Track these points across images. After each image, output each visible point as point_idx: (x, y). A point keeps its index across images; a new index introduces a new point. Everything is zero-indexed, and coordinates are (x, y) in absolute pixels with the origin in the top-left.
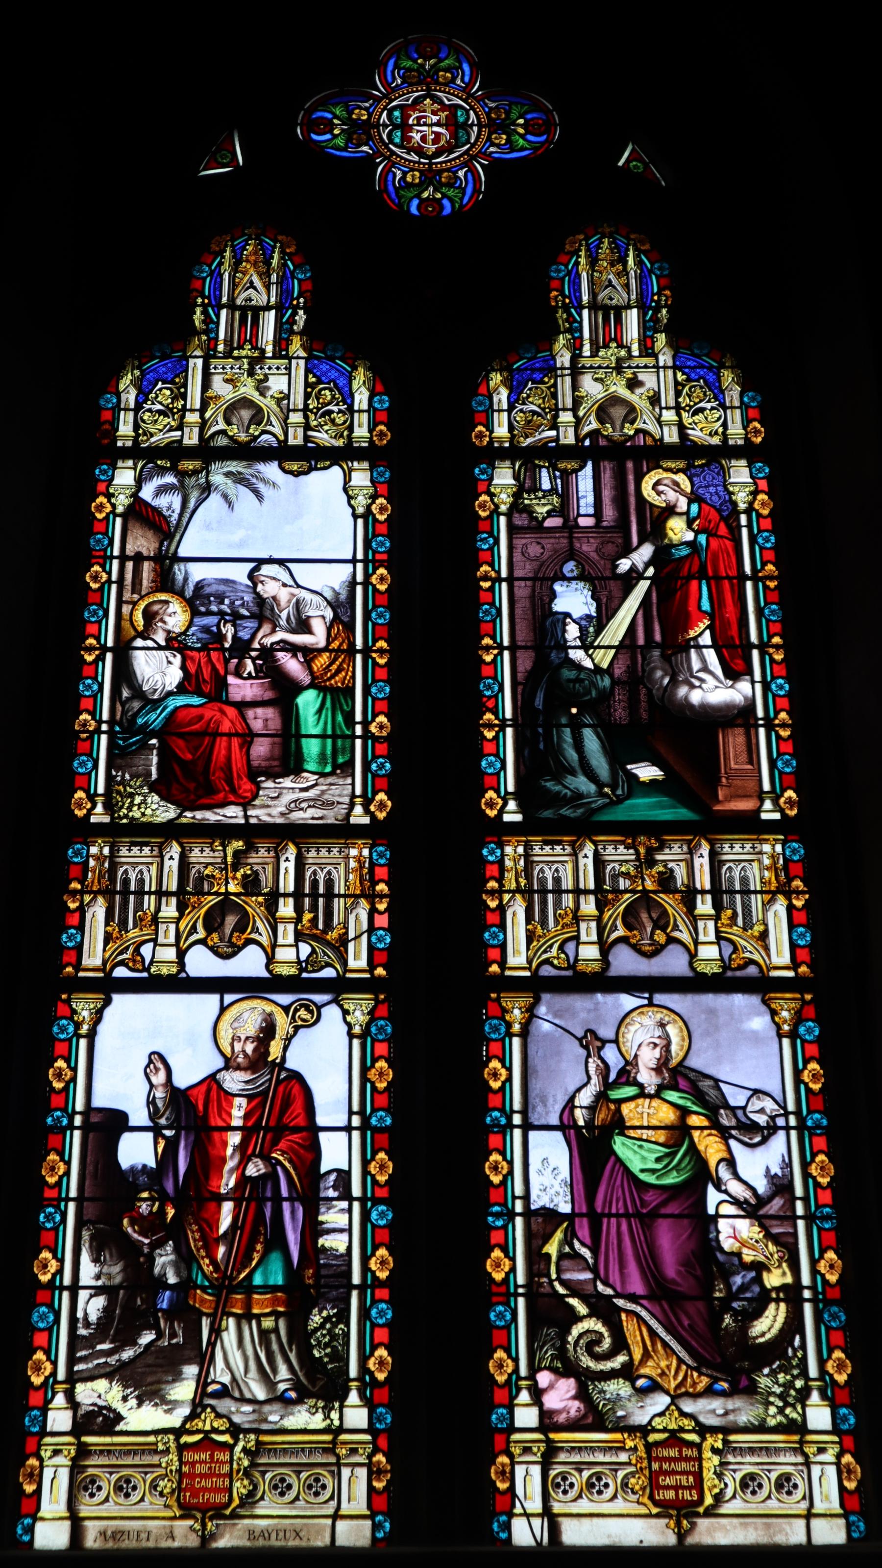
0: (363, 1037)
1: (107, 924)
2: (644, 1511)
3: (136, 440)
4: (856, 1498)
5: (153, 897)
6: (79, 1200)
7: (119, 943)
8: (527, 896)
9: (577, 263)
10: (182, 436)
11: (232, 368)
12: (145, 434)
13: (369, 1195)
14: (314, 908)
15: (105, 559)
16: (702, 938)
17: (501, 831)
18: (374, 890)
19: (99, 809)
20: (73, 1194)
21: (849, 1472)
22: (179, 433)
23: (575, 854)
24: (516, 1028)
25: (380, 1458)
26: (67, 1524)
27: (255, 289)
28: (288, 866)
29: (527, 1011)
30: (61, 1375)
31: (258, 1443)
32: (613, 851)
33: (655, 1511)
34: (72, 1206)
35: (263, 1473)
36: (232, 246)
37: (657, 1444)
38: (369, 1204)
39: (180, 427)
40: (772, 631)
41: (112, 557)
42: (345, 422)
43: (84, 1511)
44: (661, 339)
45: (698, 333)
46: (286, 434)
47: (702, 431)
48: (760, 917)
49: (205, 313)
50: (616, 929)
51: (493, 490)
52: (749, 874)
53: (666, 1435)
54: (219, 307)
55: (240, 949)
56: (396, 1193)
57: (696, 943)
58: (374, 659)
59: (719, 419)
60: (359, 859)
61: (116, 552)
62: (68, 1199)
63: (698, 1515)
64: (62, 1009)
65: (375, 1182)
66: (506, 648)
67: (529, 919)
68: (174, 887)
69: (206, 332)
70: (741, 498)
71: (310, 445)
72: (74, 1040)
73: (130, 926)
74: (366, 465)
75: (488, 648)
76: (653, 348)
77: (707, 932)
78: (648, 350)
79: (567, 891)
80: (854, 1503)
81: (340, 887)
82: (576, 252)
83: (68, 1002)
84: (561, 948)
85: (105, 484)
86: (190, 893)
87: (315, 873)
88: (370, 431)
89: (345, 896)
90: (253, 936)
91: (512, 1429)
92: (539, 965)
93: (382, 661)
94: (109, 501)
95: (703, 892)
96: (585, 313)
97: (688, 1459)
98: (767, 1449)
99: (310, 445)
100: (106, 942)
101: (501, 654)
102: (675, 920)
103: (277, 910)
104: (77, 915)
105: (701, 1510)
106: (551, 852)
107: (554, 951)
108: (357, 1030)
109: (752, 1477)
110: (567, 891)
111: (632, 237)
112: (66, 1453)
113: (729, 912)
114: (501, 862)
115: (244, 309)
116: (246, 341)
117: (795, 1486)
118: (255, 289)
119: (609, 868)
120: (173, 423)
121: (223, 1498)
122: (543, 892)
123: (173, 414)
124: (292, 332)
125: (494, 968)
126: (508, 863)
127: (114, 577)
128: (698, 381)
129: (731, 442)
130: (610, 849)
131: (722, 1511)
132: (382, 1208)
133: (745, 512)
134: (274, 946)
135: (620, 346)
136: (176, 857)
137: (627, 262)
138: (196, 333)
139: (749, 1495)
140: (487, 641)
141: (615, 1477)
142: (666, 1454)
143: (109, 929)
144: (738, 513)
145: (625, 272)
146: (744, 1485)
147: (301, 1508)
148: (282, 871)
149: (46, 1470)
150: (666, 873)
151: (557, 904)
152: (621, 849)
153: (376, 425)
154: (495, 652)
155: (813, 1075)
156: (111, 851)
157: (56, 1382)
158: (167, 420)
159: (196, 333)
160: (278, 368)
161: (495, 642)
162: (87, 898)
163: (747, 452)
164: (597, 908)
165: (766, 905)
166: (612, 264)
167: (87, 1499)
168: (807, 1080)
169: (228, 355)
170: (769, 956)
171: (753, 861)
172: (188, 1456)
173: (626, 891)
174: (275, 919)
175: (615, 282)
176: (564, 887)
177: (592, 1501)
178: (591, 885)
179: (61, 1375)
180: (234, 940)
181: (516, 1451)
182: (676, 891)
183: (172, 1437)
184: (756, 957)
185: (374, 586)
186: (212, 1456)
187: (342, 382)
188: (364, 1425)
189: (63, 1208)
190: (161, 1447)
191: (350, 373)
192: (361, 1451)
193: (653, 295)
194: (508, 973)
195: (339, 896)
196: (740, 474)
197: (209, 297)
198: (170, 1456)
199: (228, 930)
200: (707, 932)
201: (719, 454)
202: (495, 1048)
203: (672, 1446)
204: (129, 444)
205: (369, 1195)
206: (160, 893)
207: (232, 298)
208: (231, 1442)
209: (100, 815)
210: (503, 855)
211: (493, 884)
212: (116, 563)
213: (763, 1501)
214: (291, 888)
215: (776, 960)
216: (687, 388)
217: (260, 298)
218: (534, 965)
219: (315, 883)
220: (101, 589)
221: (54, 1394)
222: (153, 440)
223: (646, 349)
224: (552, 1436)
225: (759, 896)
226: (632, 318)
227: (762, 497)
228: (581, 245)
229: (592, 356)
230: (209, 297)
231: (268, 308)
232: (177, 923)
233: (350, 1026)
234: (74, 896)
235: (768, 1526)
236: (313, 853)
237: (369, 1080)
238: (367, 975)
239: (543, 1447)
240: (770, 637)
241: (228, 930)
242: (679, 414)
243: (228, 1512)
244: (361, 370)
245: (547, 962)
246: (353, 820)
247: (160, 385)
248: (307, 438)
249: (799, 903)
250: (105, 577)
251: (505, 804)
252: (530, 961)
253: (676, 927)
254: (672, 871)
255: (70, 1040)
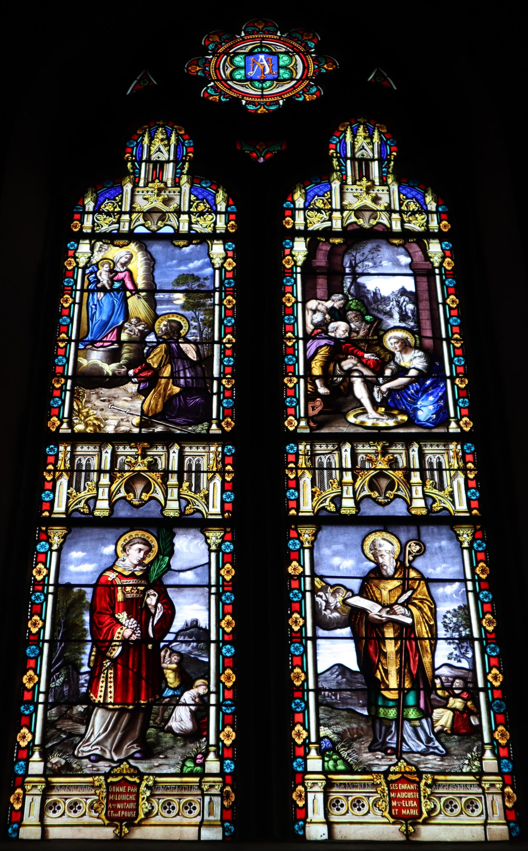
0: (217, 551)
1: (312, 487)
2: (385, 820)
3: (93, 228)
4: (513, 812)
5: (95, 473)
6: (52, 642)
7: (75, 499)
8: (69, 473)
9: (345, 137)
10: (119, 227)
11: (357, 190)
12: (98, 226)
13: (221, 639)
14: (189, 480)
15: (72, 291)
16: (414, 495)
17: (296, 437)
18: (224, 469)
19: (65, 426)
20: (47, 637)
21: (509, 797)
22: (117, 225)
23: (407, 450)
24: (55, 547)
25: (508, 790)
26: (39, 829)
27: (161, 152)
28: (174, 457)
29: (312, 536)
30: (313, 739)
31: (155, 782)
32: (123, 450)
33: (392, 820)
34: (46, 646)
35: (439, 798)
36: (351, 128)
37: (112, 783)
38: (221, 644)
39: (118, 222)
40: (227, 331)
41: (76, 290)
42: (212, 219)
43: (48, 821)
44: (184, 178)
45: (409, 172)
46: (391, 224)
47: (416, 225)
48: (205, 486)
49: (133, 164)
50: (364, 490)
51: (77, 255)
52: (442, 460)
53: (400, 775)
54: (346, 159)
55: (392, 500)
56: (236, 638)
57: (166, 499)
58: (453, 345)
59: (212, 219)
60: (216, 454)
61: (79, 287)
62: (44, 641)
63: (419, 823)
64: (293, 534)
65: (224, 632)
66: (301, 339)
67: (70, 485)
68: (108, 467)
69: (134, 173)
70: (436, 260)
71: (192, 232)
72: (49, 552)
73: (326, 488)
74: (221, 242)
75: (290, 339)
76: (179, 183)
77: (417, 491)
78: (176, 183)
79: (94, 471)
80: (512, 816)
81: (204, 468)
82: (345, 132)
83: (296, 529)
84: (86, 502)
85: (289, 250)
86: (117, 471)
87: (190, 460)
88: (226, 224)
89: (207, 472)
90: (154, 495)
91: (306, 772)
92: (319, 510)
93: (458, 345)
94: (75, 261)
95: (415, 470)
96: (349, 162)
97: (131, 793)
98: (345, 784)
99: (192, 232)
100: (313, 497)
101: (297, 342)
102: (155, 487)
103: (168, 480)
104: (51, 483)
105: (420, 821)
106: (87, 450)
107: (82, 505)
108: (213, 547)
109: (76, 803)
110: (94, 471)
111: (175, 127)
112: (320, 784)
113: (187, 484)
114: (57, 456)
115: (155, 163)
116: (363, 176)
117: (477, 807)
118: (161, 152)
119: (120, 459)
120: (114, 220)
121: (414, 812)
122: (79, 471)
123: (114, 216)
124: (182, 174)
125: (293, 512)
126: (61, 456)
127: (77, 301)
128: (412, 199)
129: (218, 232)
130: (429, 447)
131: (433, 822)
132: (228, 646)
133: (438, 268)
134: (411, 499)
135: (161, 181)
136: (177, 451)
137: (170, 140)
138: (128, 174)
139: (356, 811)
140: (290, 334)
141: (348, 800)
142: (117, 790)
143: (314, 490)
144: (434, 268)
145: (169, 145)
146: (446, 806)
147: (372, 818)
148: (411, 457)
149: (309, 794)
150: (152, 461)
151: (330, 476)
152: (128, 448)
153: (229, 221)
154: (294, 341)
155: (482, 570)
156: (72, 449)
157: (34, 745)
158: (110, 219)
159: (128, 174)
160: (383, 191)
161: (294, 335)
162: (300, 472)
163: (440, 236)
164: (421, 479)
165: (210, 480)
166: (365, 138)
167: (335, 811)
168: (478, 573)
169: (354, 183)
170: (208, 508)
171: (205, 456)
172: (393, 787)
173: (370, 469)
174: (410, 484)
175: (366, 147)
176: (92, 468)
177: (447, 815)
178: (349, 466)
179: (313, 739)
180: (143, 497)
181: (28, 787)
182: (158, 471)
183: (102, 778)
184: (201, 508)
185: (225, 306)
186: (126, 789)
187: (210, 198)
188: (496, 770)
189: (41, 646)
190: (97, 784)
191: (215, 194)
192: (320, 784)
193: (183, 156)
194: (54, 516)
195: (204, 472)
196: (435, 248)
197: (135, 156)
198: (102, 790)
199: (138, 492)
200: (173, 493)
201: (422, 238)
202: (41, 558)
203: (122, 786)
204: (89, 231)
205: (221, 639)
206: (100, 471)
207: (149, 155)
208: (138, 781)
209: (65, 429)
210: (58, 452)
211: (50, 467)
212: (78, 293)
213: (478, 816)
214: (176, 468)
215: (458, 508)
216: (195, 204)
217: (164, 157)
218: (316, 511)
219: (190, 466)
220: (293, 306)
221: (33, 753)
222: (102, 229)
223: (175, 183)
224: (330, 776)
225: (448, 472)
226: (375, 166)
227: (448, 260)
228: (347, 128)
229: (353, 184)
230: (135, 156)
231: (168, 161)
232: (110, 488)
233: (209, 545)
234: (292, 471)
235: (79, 830)
236: (429, 447)
237: (221, 575)
238: (468, 515)
239: (324, 783)
240: (453, 334)
241: (138, 492)
242: (401, 216)
243: (136, 822)
244: (221, 192)
245: (324, 508)
246: (211, 432)
247: (316, 197)
248: (190, 228)
249: (228, 479)
250: (293, 300)
251: (299, 423)
252: (313, 508)
253: (155, 491)
254: (396, 458)
255: (46, 553)
